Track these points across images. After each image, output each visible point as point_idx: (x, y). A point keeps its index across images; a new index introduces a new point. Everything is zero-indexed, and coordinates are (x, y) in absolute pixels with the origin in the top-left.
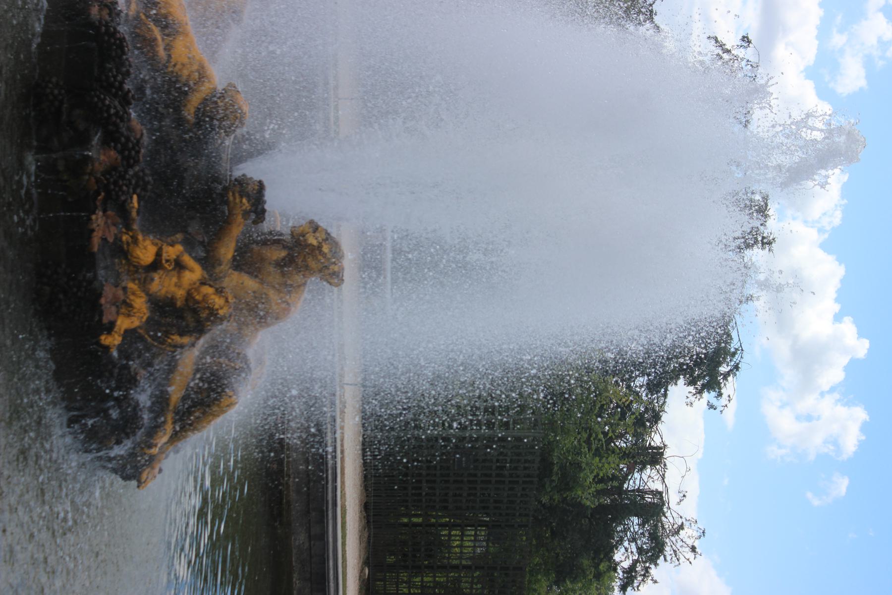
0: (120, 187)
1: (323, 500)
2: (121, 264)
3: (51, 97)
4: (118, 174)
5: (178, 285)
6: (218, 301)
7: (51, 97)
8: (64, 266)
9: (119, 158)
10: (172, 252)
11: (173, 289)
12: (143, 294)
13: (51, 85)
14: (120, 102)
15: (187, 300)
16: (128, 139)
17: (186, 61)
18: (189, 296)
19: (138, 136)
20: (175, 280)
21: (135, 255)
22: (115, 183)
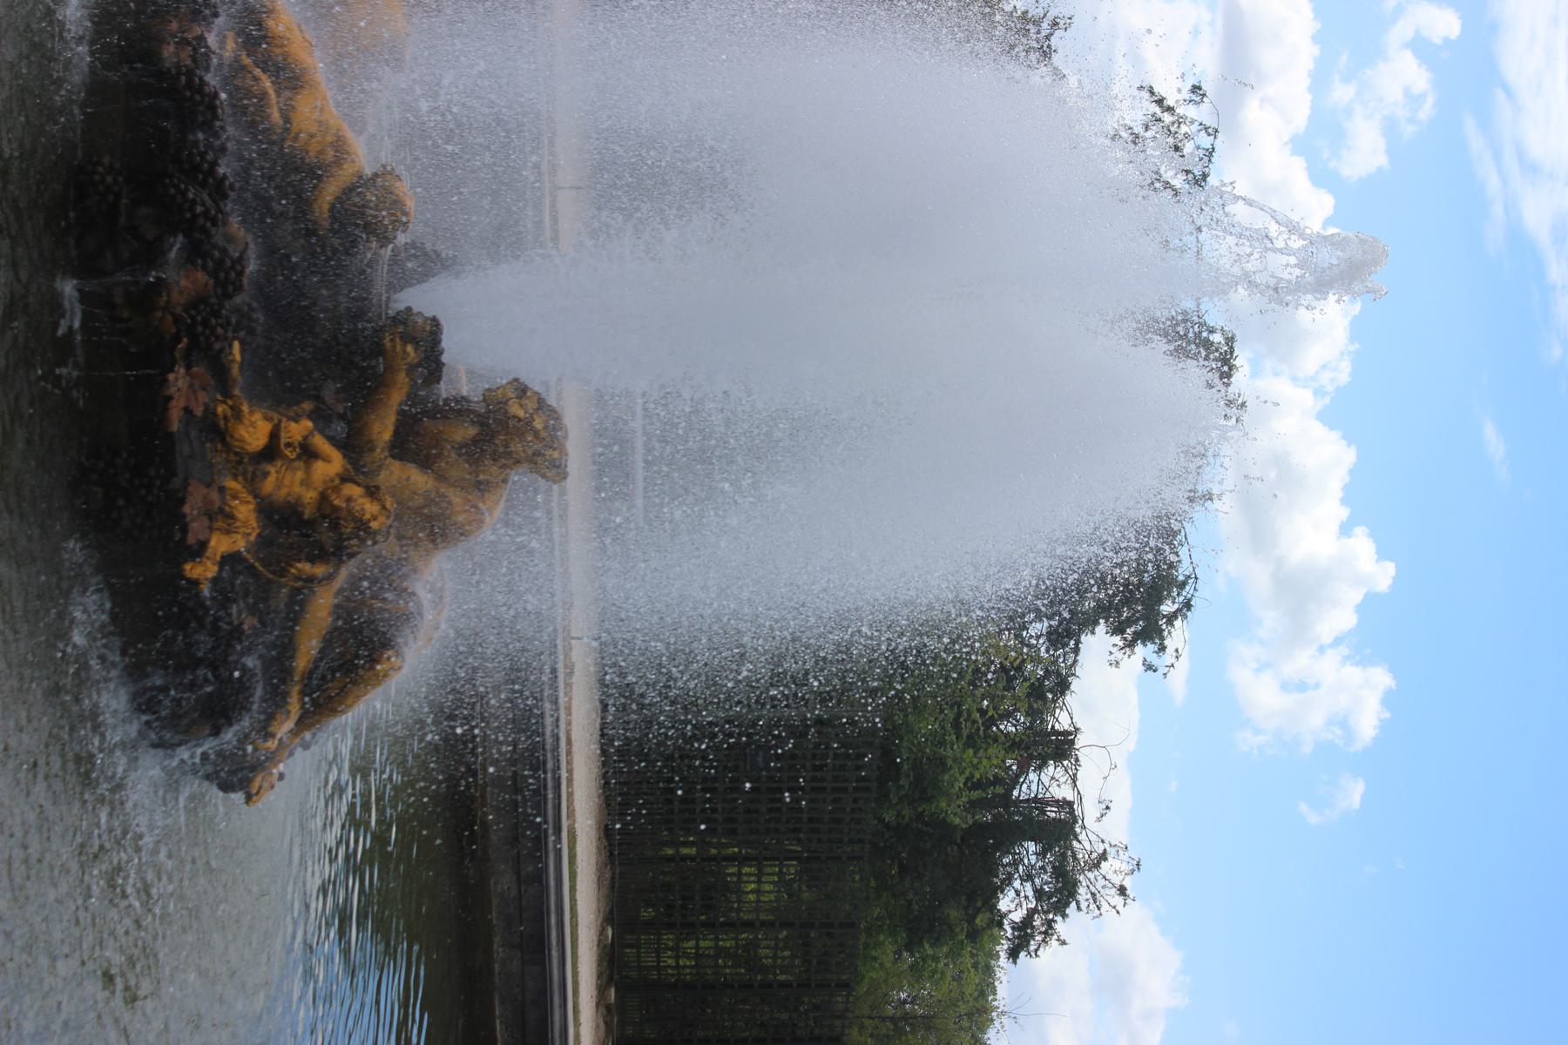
5: (306, 483)
6: (369, 508)
7: (101, 188)
10: (297, 429)
11: (297, 489)
16: (224, 251)
17: (314, 129)
18: (324, 498)
20: (300, 475)
21: (237, 436)
22: (205, 323)
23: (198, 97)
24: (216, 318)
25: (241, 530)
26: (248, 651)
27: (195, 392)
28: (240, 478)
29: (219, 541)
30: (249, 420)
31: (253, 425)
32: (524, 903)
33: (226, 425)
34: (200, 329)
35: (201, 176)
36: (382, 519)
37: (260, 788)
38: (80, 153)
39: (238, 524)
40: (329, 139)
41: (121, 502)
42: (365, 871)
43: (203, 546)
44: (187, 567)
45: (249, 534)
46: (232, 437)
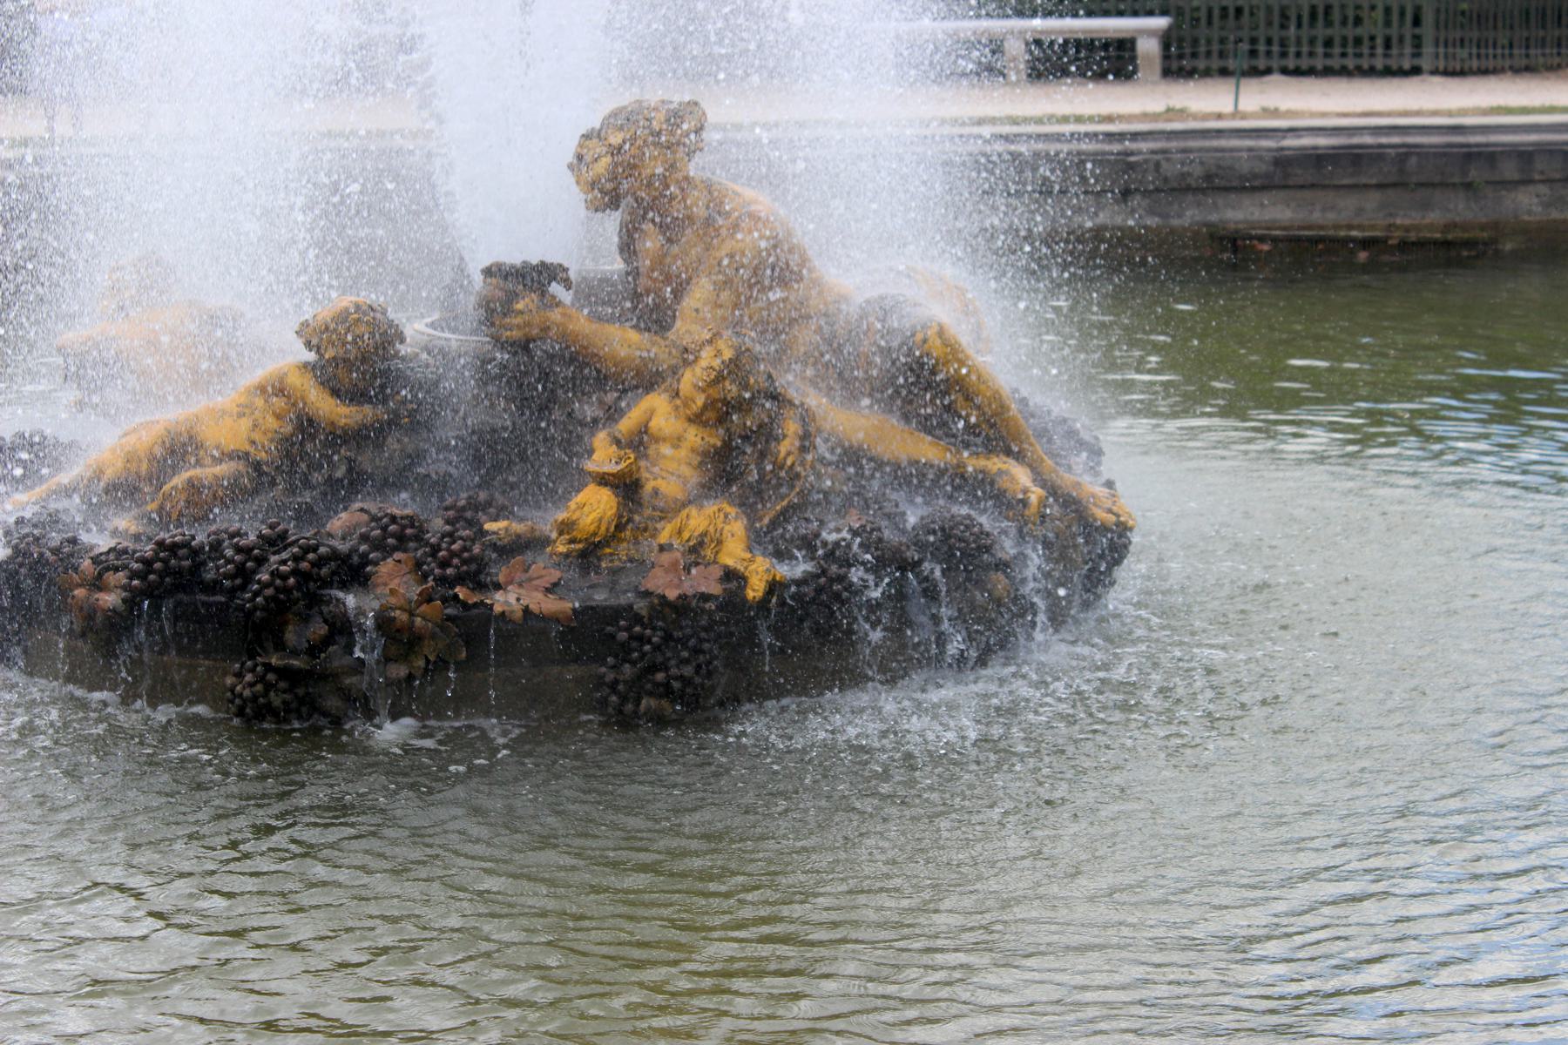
0: (453, 554)
1: (1443, 155)
2: (611, 554)
3: (259, 687)
4: (429, 559)
5: (677, 441)
6: (708, 359)
7: (259, 687)
8: (603, 669)
9: (398, 555)
10: (603, 456)
11: (683, 453)
12: (684, 513)
13: (238, 688)
14: (274, 553)
15: (705, 424)
16: (364, 538)
17: (245, 424)
18: (696, 419)
19: (365, 517)
20: (666, 450)
21: (592, 528)
22: (444, 564)
23: (158, 565)
24: (440, 550)
25: (720, 526)
26: (895, 518)
27: (530, 580)
28: (658, 526)
29: (730, 555)
30: (574, 511)
31: (581, 506)
32: (1558, 176)
33: (580, 541)
34: (449, 571)
35: (249, 564)
36: (721, 344)
37: (1110, 511)
38: (200, 709)
39: (711, 529)
40: (260, 402)
41: (660, 676)
42: (1281, 389)
43: (730, 575)
44: (750, 594)
45: (726, 516)
46: (595, 534)
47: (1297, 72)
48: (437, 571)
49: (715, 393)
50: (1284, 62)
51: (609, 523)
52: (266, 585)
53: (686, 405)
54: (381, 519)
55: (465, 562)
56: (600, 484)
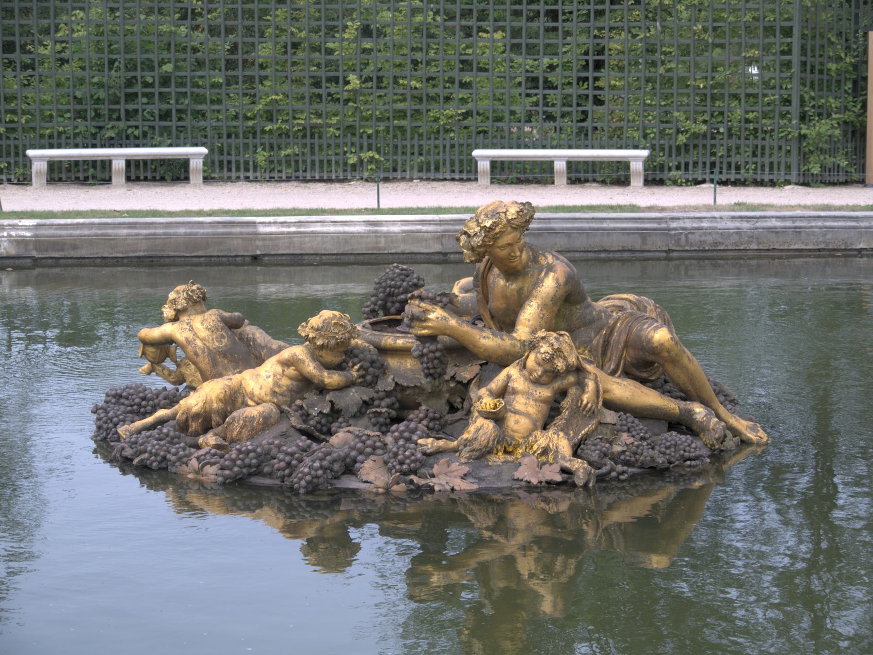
9: (373, 457)
22: (401, 463)
34: (405, 467)
47: (305, 181)
48: (398, 467)
49: (548, 367)
50: (712, 176)
51: (494, 440)
52: (306, 474)
53: (531, 374)
54: (361, 436)
55: (413, 461)
56: (486, 418)
